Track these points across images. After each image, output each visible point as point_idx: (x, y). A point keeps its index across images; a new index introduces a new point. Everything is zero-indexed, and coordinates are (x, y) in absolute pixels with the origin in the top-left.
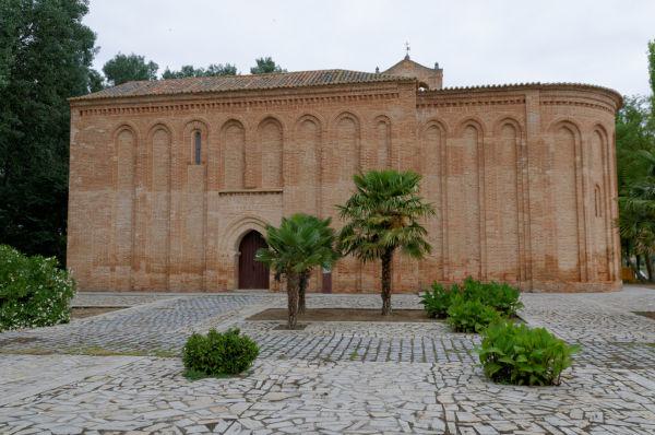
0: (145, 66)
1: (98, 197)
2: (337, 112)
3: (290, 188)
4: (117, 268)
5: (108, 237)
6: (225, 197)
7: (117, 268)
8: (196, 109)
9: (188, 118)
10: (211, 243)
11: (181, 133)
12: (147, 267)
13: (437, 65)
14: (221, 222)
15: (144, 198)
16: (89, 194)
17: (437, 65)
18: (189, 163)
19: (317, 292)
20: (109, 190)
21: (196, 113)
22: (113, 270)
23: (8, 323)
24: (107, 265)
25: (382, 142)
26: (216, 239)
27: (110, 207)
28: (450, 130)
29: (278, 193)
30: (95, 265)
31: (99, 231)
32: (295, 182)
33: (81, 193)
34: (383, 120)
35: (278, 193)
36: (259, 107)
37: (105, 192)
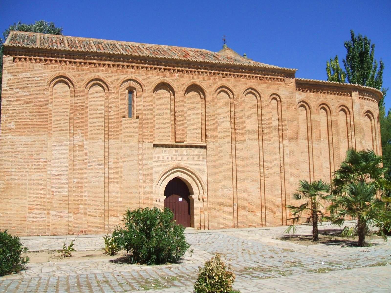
0: (20, 256)
1: (34, 142)
2: (245, 87)
3: (212, 143)
4: (52, 212)
5: (44, 182)
6: (157, 149)
7: (52, 212)
8: (131, 70)
9: (125, 77)
10: (147, 188)
11: (118, 90)
12: (85, 210)
13: (359, 34)
14: (154, 170)
15: (81, 146)
16: (24, 139)
17: (359, 34)
18: (124, 117)
19: (277, 239)
20: (45, 137)
21: (131, 73)
22: (48, 214)
23: (1, 218)
24: (44, 209)
25: (275, 113)
26: (151, 185)
27: (46, 152)
28: (313, 109)
29: (201, 147)
30: (31, 209)
31: (35, 177)
32: (215, 139)
33: (14, 138)
34: (275, 97)
35: (201, 147)
36: (186, 74)
37: (43, 138)
